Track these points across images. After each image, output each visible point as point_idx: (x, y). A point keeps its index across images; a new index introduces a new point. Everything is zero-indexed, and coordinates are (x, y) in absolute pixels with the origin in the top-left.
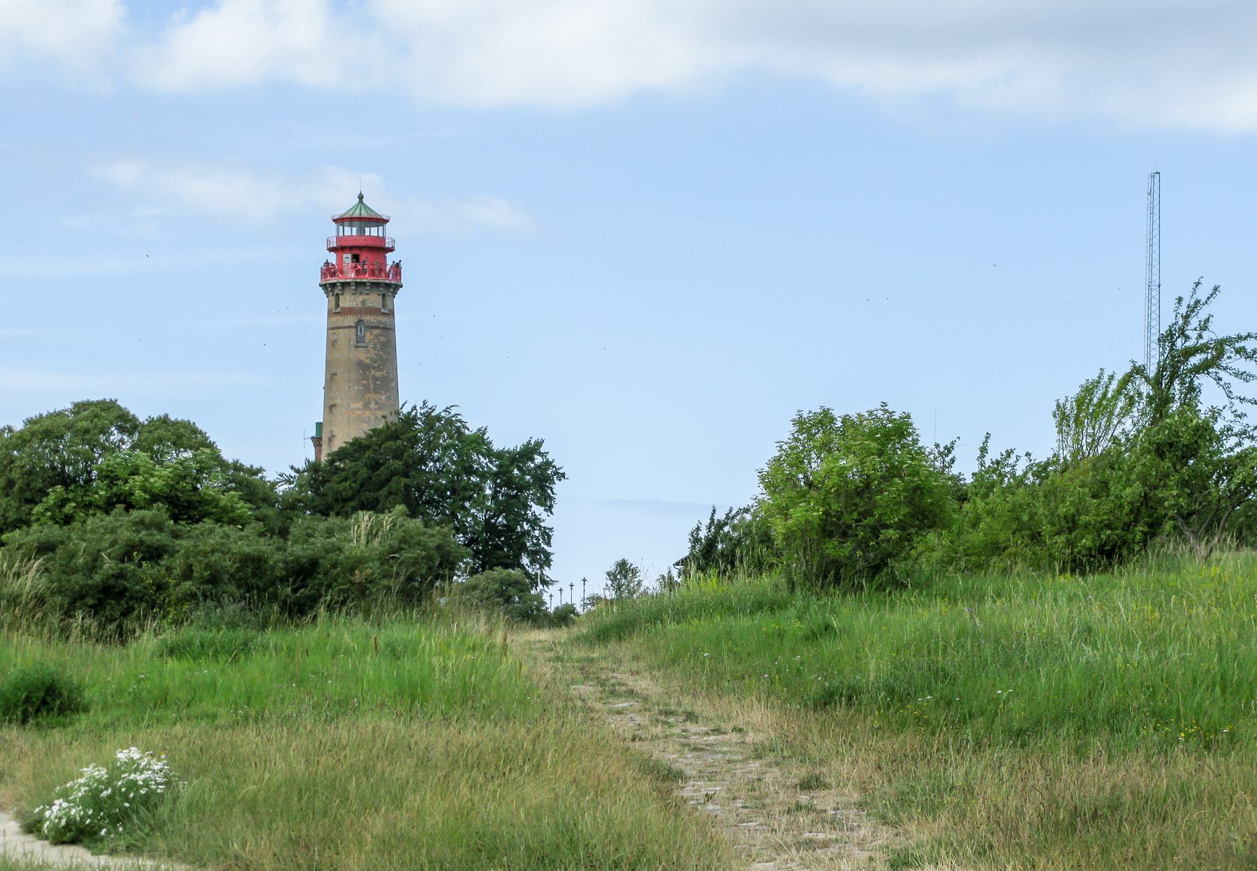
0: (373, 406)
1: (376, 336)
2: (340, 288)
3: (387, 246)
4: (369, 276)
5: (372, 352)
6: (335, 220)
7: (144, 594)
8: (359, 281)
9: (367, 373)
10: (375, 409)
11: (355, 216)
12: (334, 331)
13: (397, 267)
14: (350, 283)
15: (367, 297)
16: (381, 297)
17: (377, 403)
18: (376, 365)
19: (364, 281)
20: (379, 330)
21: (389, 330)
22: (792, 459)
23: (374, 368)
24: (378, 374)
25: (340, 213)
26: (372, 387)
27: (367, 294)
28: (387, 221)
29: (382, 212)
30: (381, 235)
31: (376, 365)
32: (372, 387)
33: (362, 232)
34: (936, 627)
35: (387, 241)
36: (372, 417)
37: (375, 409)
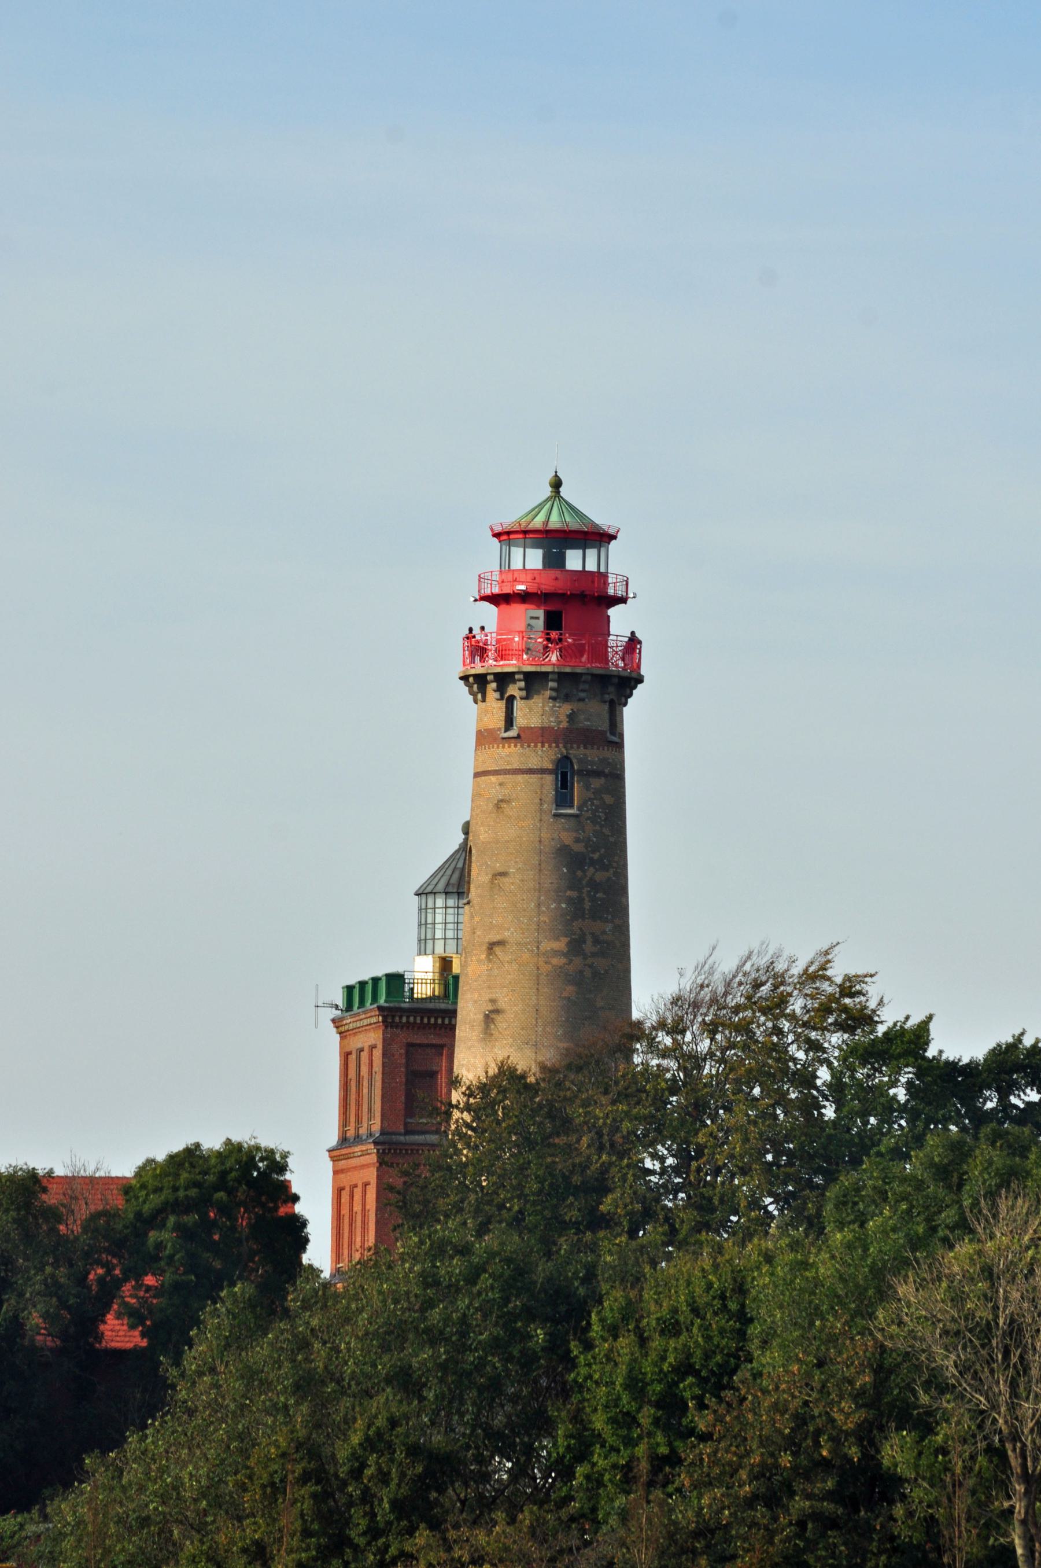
0: (589, 947)
1: (597, 792)
2: (522, 684)
3: (611, 591)
4: (590, 660)
5: (589, 827)
6: (497, 535)
7: (21, 1295)
8: (568, 670)
9: (579, 873)
10: (594, 955)
11: (531, 527)
12: (501, 778)
13: (633, 642)
14: (546, 674)
15: (581, 705)
16: (606, 707)
17: (596, 941)
18: (596, 856)
19: (578, 670)
20: (602, 780)
21: (615, 777)
22: (995, 1048)
23: (593, 863)
24: (600, 876)
25: (510, 517)
26: (587, 905)
27: (581, 700)
28: (614, 537)
29: (602, 518)
30: (602, 570)
31: (596, 856)
32: (587, 905)
33: (554, 561)
34: (622, 1381)
35: (611, 579)
36: (588, 973)
37: (594, 955)
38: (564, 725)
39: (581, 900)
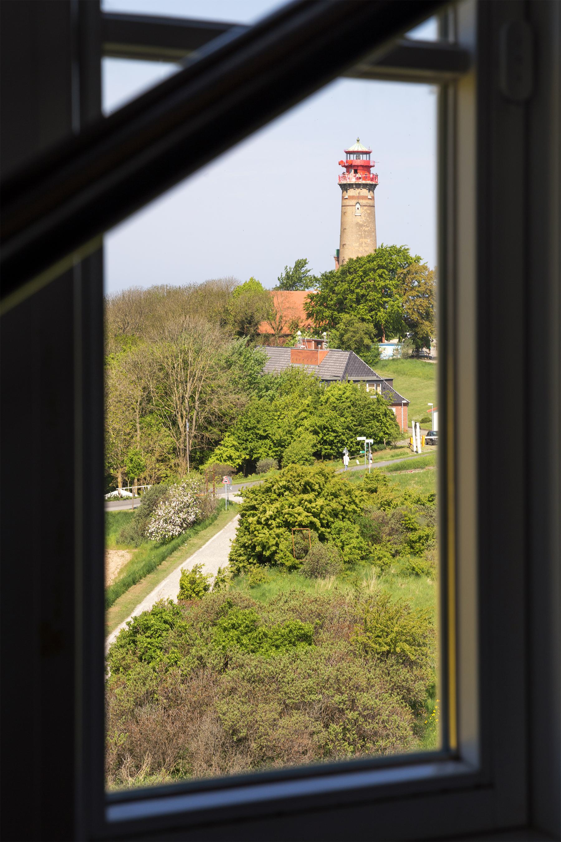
18: (365, 224)
23: (364, 226)
26: (363, 235)
32: (363, 235)
38: (358, 195)
39: (362, 234)
